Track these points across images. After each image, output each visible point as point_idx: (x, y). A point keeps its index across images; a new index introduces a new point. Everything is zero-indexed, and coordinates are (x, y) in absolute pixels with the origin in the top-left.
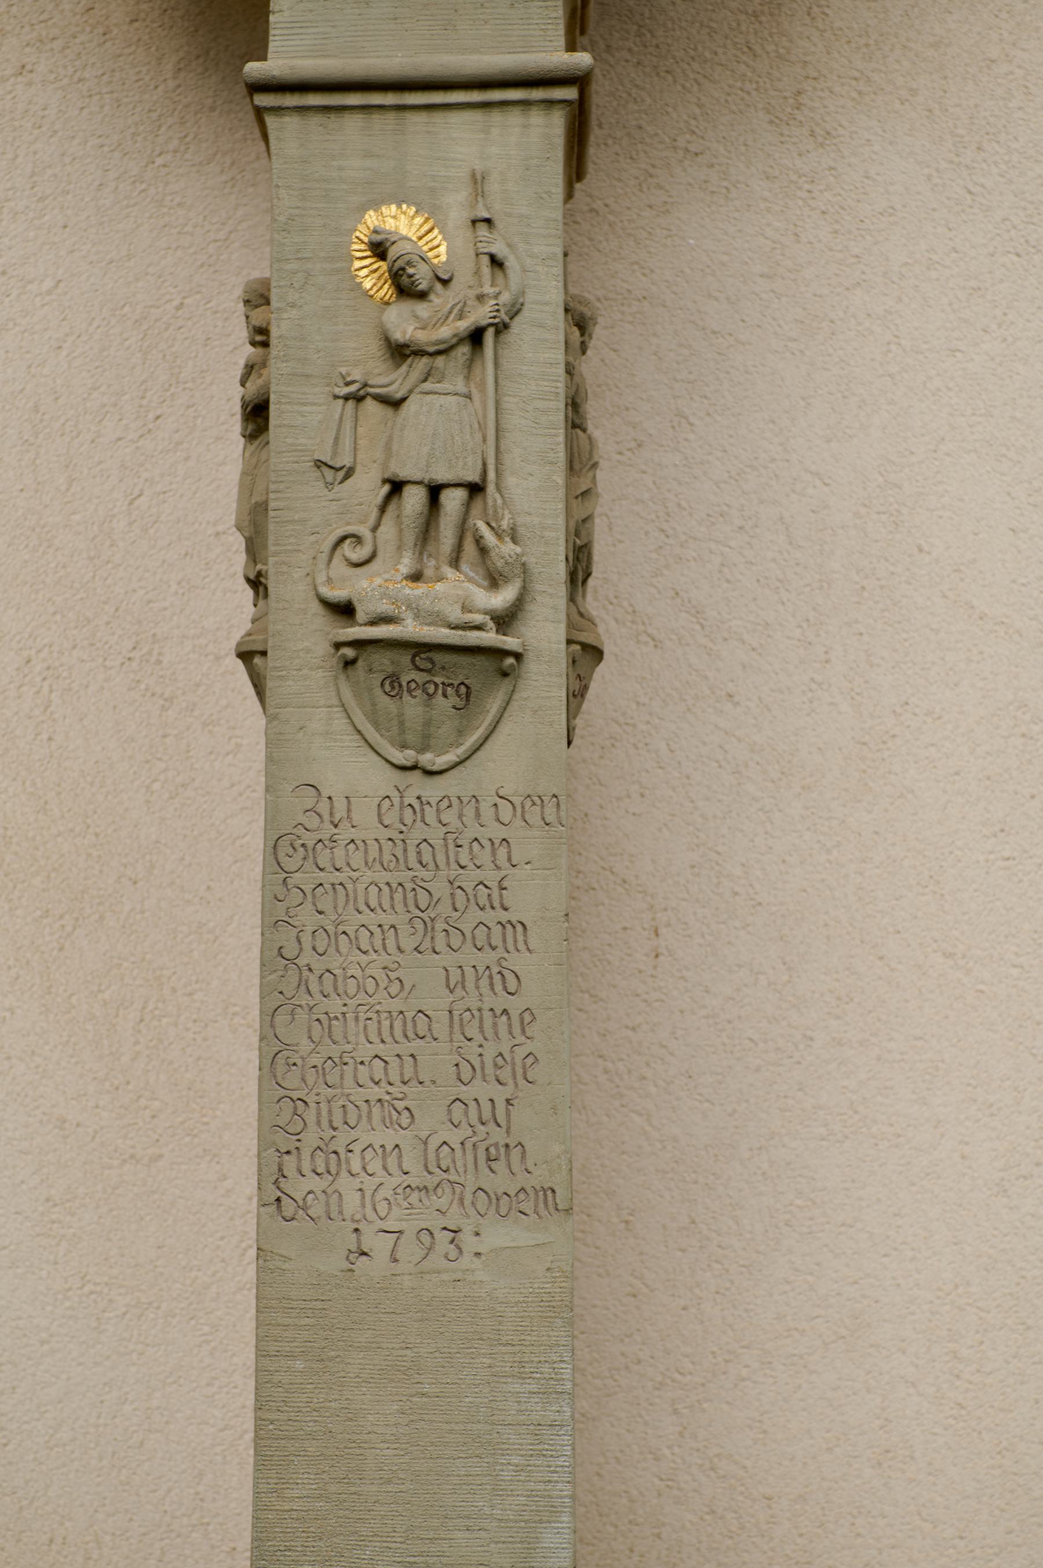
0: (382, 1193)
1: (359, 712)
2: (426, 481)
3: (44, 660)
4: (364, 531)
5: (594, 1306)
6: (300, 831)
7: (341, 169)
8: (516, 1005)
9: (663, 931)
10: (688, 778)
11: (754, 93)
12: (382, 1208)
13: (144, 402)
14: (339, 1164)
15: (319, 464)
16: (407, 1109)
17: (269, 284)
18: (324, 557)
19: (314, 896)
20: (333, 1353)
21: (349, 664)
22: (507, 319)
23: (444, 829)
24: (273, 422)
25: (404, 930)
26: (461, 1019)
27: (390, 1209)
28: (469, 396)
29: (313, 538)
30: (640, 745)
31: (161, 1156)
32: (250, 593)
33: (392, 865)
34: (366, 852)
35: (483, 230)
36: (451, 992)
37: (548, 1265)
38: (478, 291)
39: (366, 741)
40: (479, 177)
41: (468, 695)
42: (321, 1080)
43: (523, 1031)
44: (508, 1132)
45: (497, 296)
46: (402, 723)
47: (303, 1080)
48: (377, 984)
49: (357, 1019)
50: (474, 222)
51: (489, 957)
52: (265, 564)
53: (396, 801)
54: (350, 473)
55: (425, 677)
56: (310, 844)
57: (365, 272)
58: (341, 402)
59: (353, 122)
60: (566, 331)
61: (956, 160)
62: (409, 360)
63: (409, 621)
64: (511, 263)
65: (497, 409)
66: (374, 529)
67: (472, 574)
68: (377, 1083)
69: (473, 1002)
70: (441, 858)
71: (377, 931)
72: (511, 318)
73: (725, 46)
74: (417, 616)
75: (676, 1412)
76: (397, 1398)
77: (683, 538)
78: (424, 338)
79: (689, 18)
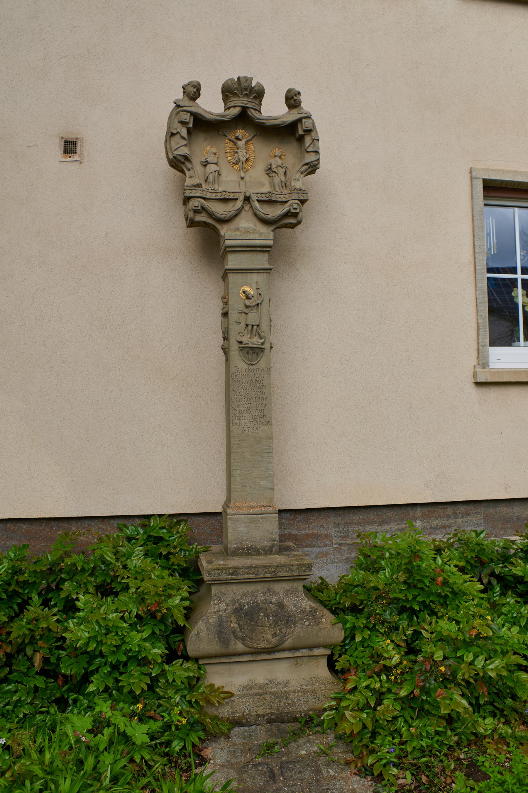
4: (243, 331)
8: (264, 396)
15: (236, 322)
21: (241, 350)
51: (261, 390)
59: (240, 275)
78: (251, 305)
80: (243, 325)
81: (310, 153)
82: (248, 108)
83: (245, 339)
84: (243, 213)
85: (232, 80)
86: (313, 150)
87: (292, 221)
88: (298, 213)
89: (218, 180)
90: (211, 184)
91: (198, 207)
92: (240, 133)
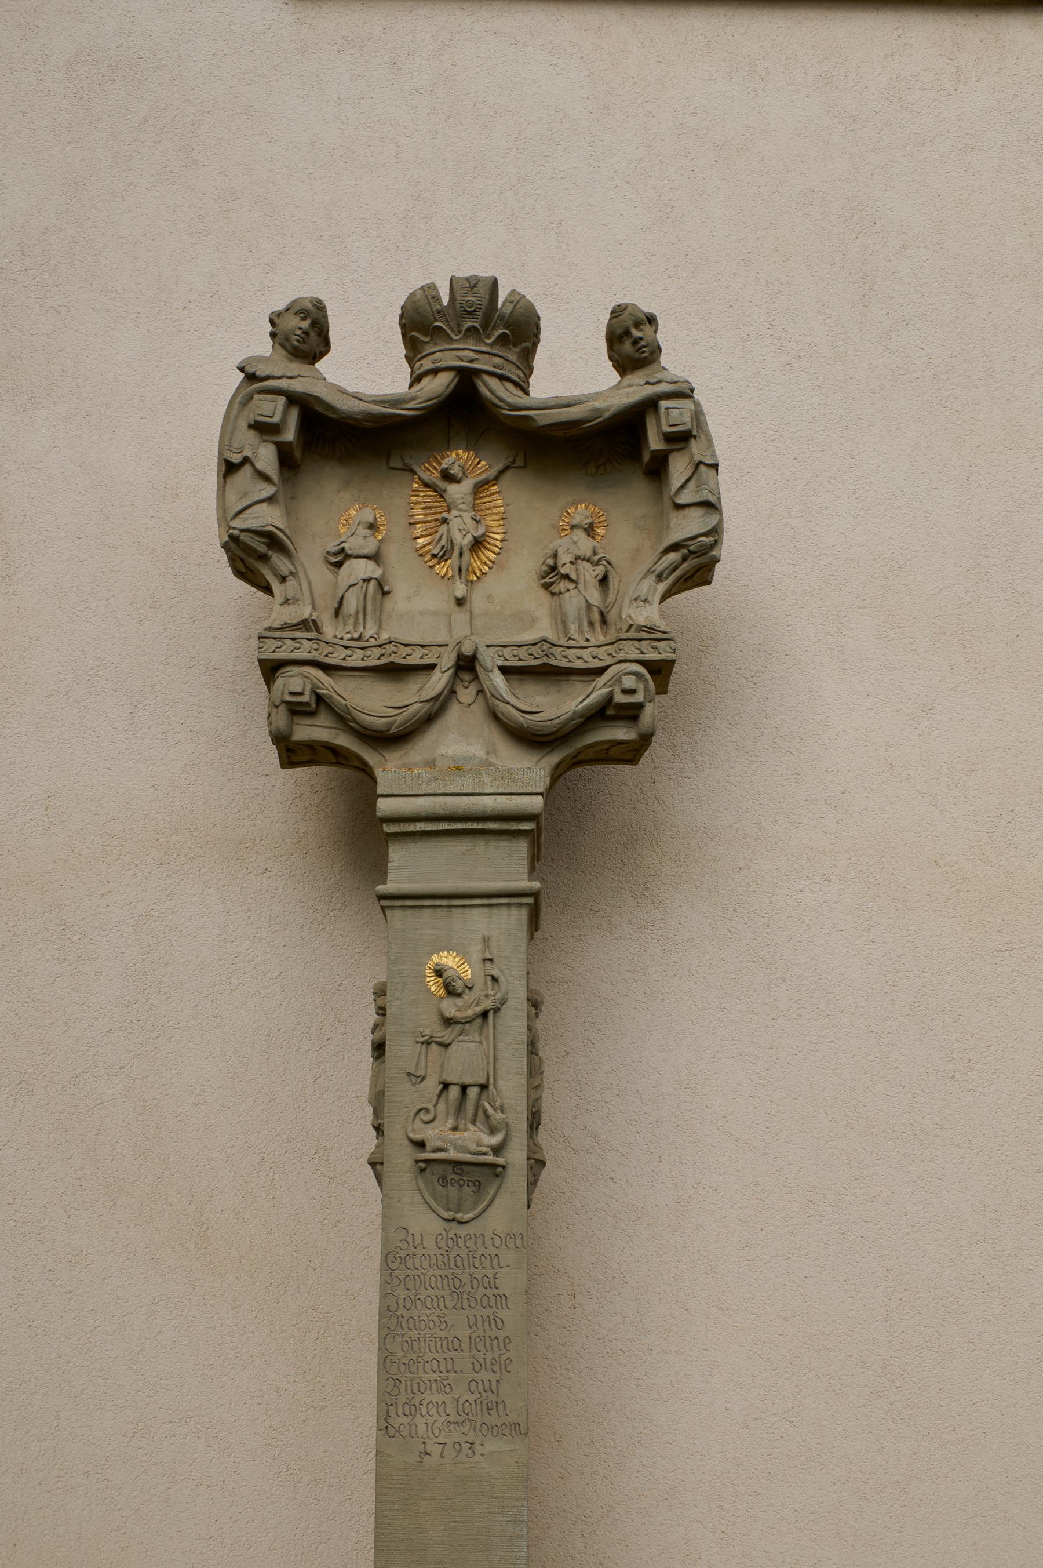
0: (436, 1425)
1: (427, 1193)
3: (271, 1158)
4: (430, 1106)
5: (542, 1483)
6: (399, 1250)
7: (421, 934)
9: (578, 1296)
10: (591, 1219)
11: (624, 882)
12: (436, 1432)
13: (322, 1032)
14: (416, 1411)
15: (409, 1074)
16: (449, 1384)
17: (386, 985)
18: (411, 1118)
19: (405, 1281)
20: (412, 1502)
21: (422, 1170)
22: (499, 1006)
23: (467, 1250)
24: (387, 1053)
25: (448, 1298)
26: (475, 1342)
27: (440, 1432)
28: (481, 1043)
29: (405, 1110)
30: (567, 1203)
31: (327, 1406)
32: (374, 1132)
33: (443, 1267)
34: (430, 1260)
35: (488, 964)
36: (470, 1328)
37: (516, 1460)
38: (486, 992)
39: (430, 1207)
40: (487, 939)
41: (479, 1186)
42: (407, 1370)
43: (505, 1348)
44: (497, 1396)
45: (494, 995)
46: (447, 1199)
47: (399, 1370)
48: (435, 1324)
49: (425, 1341)
50: (484, 960)
51: (489, 1312)
52: (383, 1120)
53: (445, 1236)
54: (424, 1078)
55: (459, 1177)
56: (403, 1256)
57: (432, 983)
58: (420, 1045)
59: (427, 913)
60: (528, 1010)
61: (723, 916)
62: (453, 1026)
63: (451, 1151)
64: (502, 979)
65: (494, 1048)
66: (435, 1106)
67: (482, 1127)
68: (434, 1372)
69: (481, 1333)
70: (466, 1264)
71: (435, 1299)
72: (502, 1005)
73: (609, 859)
74: (455, 1148)
75: (583, 1536)
76: (442, 1523)
78: (459, 1015)
79: (592, 846)
80: (432, 1085)
81: (687, 511)
82: (478, 372)
83: (435, 1134)
84: (454, 712)
85: (430, 291)
86: (698, 499)
87: (622, 733)
88: (640, 706)
89: (380, 609)
90: (352, 621)
91: (301, 694)
92: (456, 458)
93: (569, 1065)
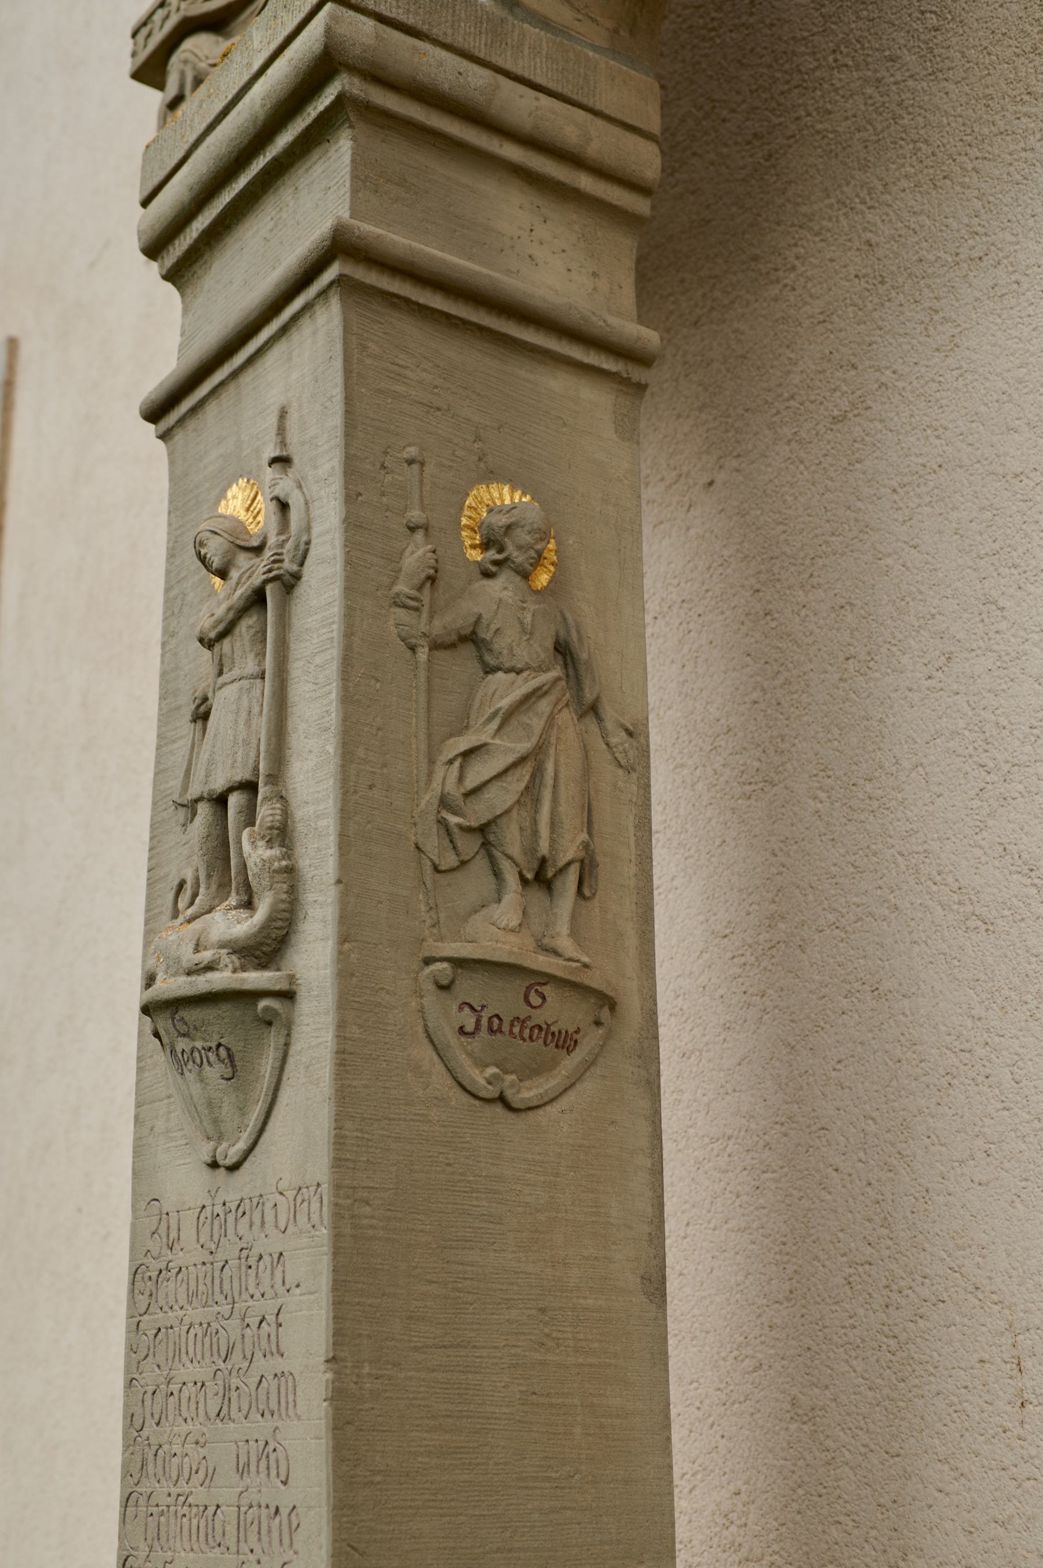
2: (205, 795)
9: (1027, 1363)
30: (980, 1079)
72: (302, 564)
77: (1006, 768)
93: (955, 687)
